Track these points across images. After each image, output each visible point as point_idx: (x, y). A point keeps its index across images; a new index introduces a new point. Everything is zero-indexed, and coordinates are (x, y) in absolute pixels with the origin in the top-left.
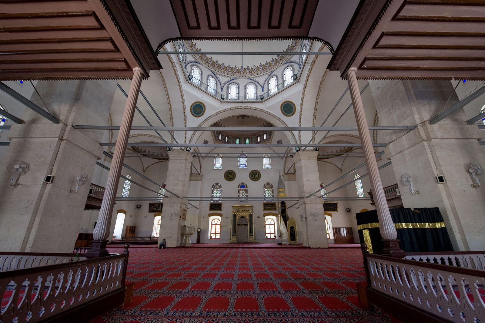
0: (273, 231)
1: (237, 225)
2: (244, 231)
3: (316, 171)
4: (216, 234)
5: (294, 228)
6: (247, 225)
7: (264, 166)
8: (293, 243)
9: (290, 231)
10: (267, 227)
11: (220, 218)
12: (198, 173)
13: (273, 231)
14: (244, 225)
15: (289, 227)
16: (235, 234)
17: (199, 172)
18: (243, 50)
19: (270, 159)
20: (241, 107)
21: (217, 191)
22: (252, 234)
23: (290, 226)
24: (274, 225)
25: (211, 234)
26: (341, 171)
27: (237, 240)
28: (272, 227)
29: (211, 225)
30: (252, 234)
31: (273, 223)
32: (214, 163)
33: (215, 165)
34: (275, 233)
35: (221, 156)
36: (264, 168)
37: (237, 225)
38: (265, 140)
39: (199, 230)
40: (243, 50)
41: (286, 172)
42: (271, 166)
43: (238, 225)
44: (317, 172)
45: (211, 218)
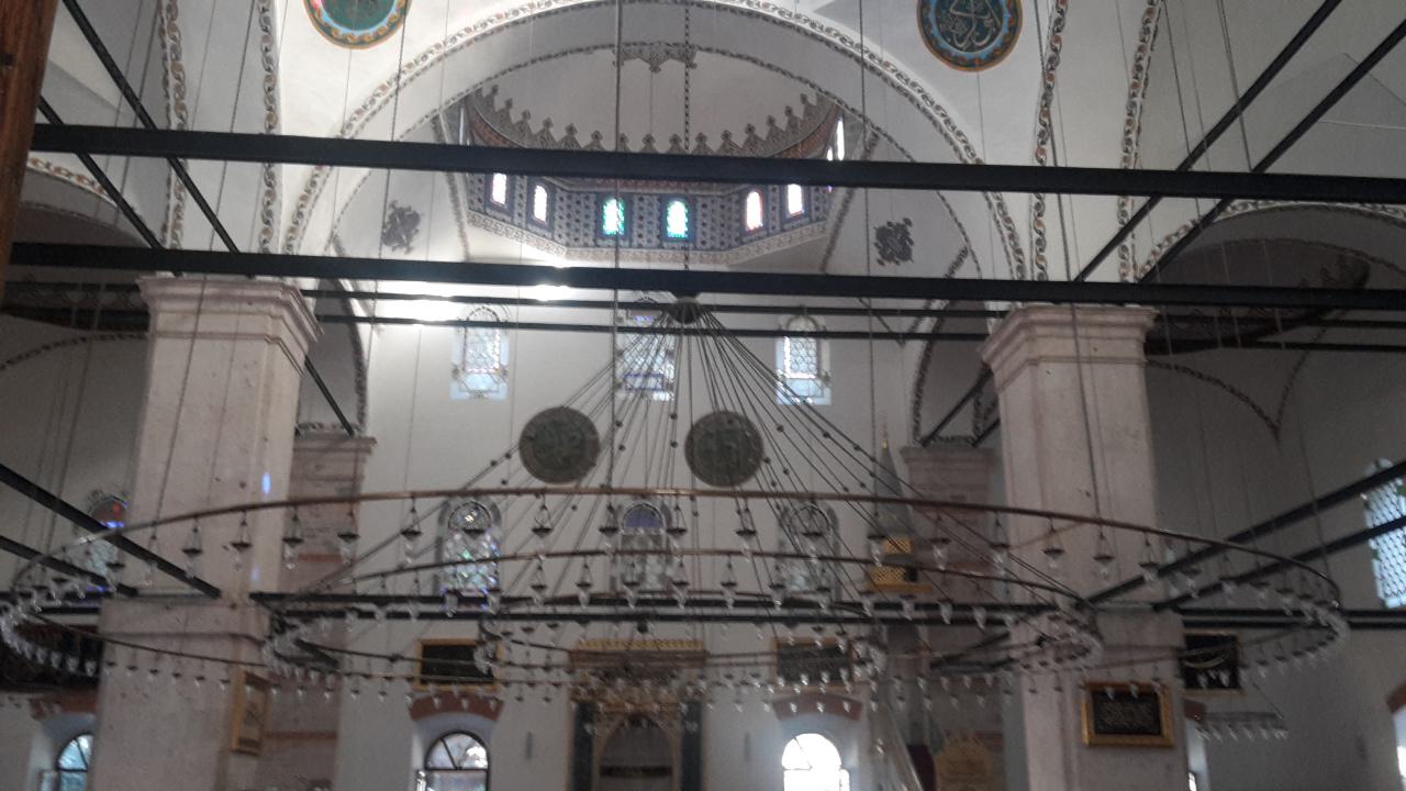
6: (663, 771)
12: (345, 424)
17: (351, 418)
26: (1275, 430)
41: (926, 430)
42: (827, 391)
43: (609, 772)
44: (1144, 444)
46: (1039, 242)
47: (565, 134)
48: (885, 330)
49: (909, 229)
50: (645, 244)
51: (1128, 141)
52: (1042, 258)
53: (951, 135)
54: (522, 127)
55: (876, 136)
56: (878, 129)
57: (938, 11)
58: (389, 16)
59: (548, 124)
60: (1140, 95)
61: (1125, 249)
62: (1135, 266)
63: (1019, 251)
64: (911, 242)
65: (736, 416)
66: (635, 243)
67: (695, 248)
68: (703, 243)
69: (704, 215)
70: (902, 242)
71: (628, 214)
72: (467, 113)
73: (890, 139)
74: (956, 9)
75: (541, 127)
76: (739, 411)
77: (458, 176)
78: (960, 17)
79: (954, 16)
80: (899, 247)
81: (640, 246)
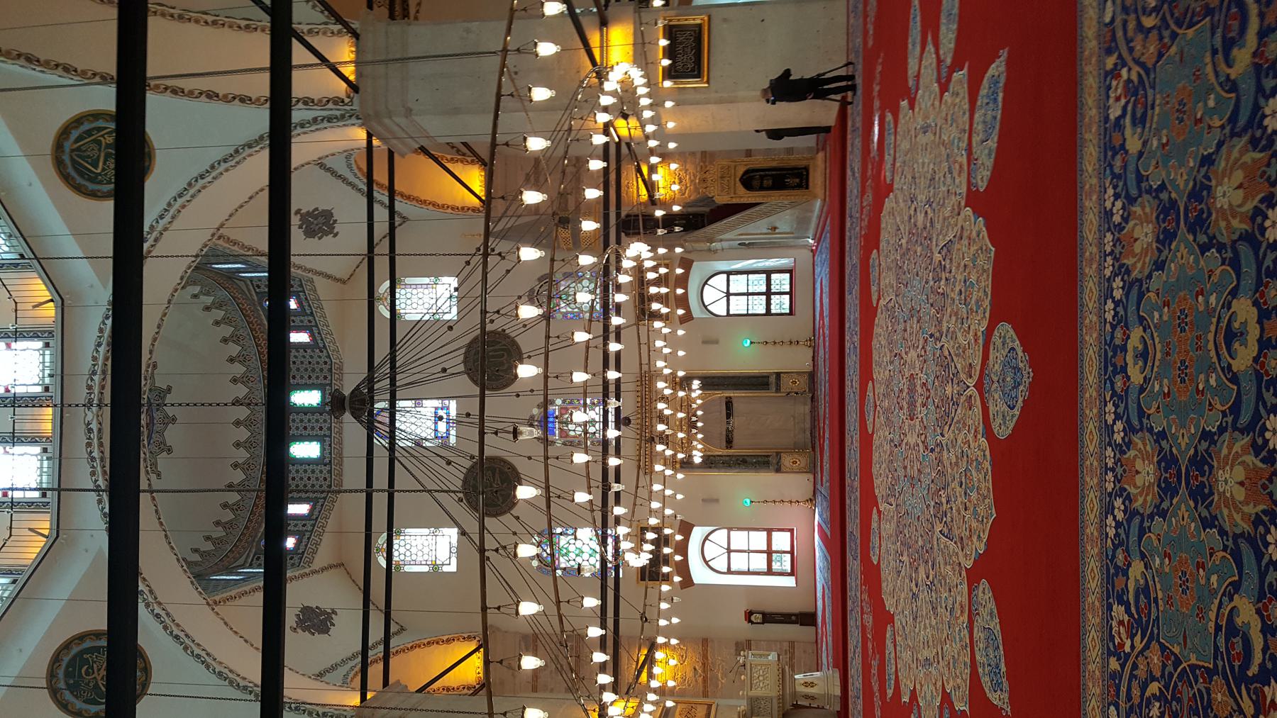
0: (758, 283)
1: (731, 452)
2: (762, 419)
3: (468, 31)
4: (769, 552)
5: (746, 172)
6: (729, 403)
7: (446, 569)
8: (818, 178)
9: (762, 188)
10: (738, 305)
11: (698, 533)
13: (758, 283)
14: (729, 415)
15: (744, 196)
16: (773, 460)
18: (356, 491)
19: (408, 280)
20: (94, 426)
21: (572, 548)
22: (773, 379)
23: (741, 190)
24: (729, 273)
25: (770, 572)
27: (796, 448)
28: (738, 283)
29: (729, 572)
30: (773, 379)
31: (720, 281)
32: (425, 569)
33: (435, 566)
34: (768, 273)
35: (387, 283)
36: (453, 568)
37: (731, 452)
38: (312, 335)
39: (757, 618)
40: (356, 491)
45: (700, 575)
46: (306, 103)
47: (220, 528)
48: (387, 240)
49: (303, 211)
50: (327, 425)
51: (214, 23)
52: (320, 101)
53: (214, 174)
54: (245, 467)
55: (220, 238)
56: (213, 235)
57: (100, 183)
58: (70, 656)
59: (238, 445)
60: (172, 11)
61: (310, 31)
62: (326, 23)
63: (315, 120)
64: (317, 209)
65: (466, 358)
66: (327, 433)
67: (330, 385)
68: (325, 378)
69: (302, 377)
70: (316, 218)
71: (302, 438)
72: (215, 573)
73: (222, 226)
74: (96, 167)
75: (220, 528)
76: (463, 351)
77: (289, 574)
78: (104, 163)
79: (103, 170)
80: (321, 220)
81: (330, 429)
